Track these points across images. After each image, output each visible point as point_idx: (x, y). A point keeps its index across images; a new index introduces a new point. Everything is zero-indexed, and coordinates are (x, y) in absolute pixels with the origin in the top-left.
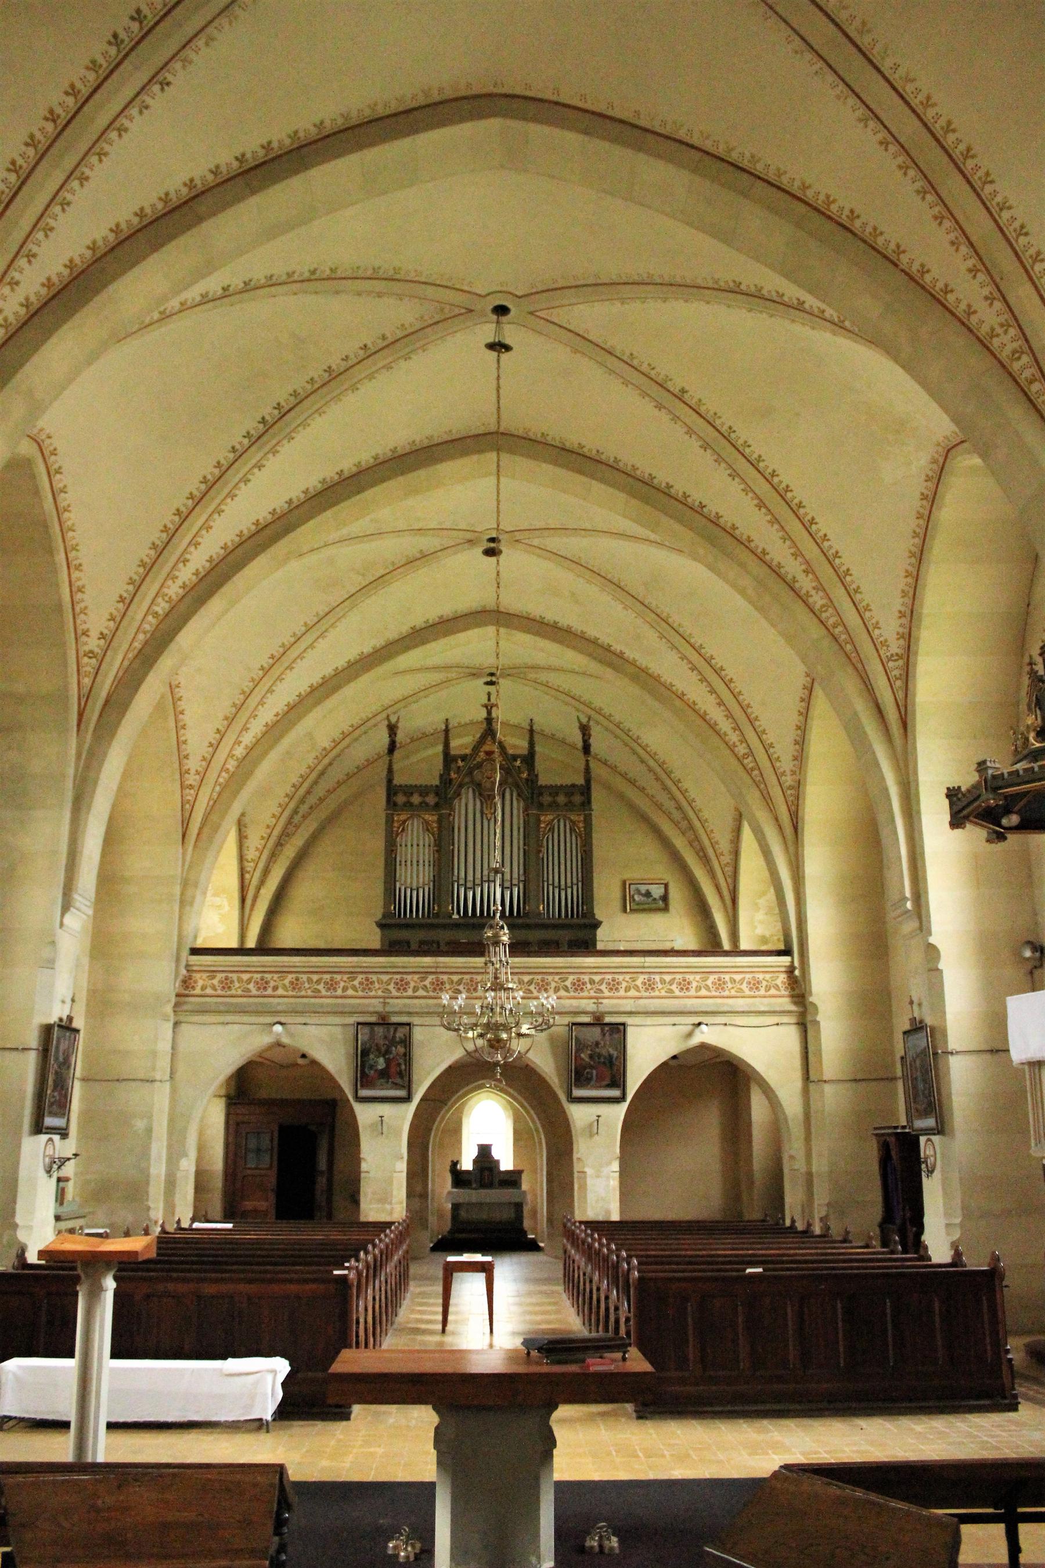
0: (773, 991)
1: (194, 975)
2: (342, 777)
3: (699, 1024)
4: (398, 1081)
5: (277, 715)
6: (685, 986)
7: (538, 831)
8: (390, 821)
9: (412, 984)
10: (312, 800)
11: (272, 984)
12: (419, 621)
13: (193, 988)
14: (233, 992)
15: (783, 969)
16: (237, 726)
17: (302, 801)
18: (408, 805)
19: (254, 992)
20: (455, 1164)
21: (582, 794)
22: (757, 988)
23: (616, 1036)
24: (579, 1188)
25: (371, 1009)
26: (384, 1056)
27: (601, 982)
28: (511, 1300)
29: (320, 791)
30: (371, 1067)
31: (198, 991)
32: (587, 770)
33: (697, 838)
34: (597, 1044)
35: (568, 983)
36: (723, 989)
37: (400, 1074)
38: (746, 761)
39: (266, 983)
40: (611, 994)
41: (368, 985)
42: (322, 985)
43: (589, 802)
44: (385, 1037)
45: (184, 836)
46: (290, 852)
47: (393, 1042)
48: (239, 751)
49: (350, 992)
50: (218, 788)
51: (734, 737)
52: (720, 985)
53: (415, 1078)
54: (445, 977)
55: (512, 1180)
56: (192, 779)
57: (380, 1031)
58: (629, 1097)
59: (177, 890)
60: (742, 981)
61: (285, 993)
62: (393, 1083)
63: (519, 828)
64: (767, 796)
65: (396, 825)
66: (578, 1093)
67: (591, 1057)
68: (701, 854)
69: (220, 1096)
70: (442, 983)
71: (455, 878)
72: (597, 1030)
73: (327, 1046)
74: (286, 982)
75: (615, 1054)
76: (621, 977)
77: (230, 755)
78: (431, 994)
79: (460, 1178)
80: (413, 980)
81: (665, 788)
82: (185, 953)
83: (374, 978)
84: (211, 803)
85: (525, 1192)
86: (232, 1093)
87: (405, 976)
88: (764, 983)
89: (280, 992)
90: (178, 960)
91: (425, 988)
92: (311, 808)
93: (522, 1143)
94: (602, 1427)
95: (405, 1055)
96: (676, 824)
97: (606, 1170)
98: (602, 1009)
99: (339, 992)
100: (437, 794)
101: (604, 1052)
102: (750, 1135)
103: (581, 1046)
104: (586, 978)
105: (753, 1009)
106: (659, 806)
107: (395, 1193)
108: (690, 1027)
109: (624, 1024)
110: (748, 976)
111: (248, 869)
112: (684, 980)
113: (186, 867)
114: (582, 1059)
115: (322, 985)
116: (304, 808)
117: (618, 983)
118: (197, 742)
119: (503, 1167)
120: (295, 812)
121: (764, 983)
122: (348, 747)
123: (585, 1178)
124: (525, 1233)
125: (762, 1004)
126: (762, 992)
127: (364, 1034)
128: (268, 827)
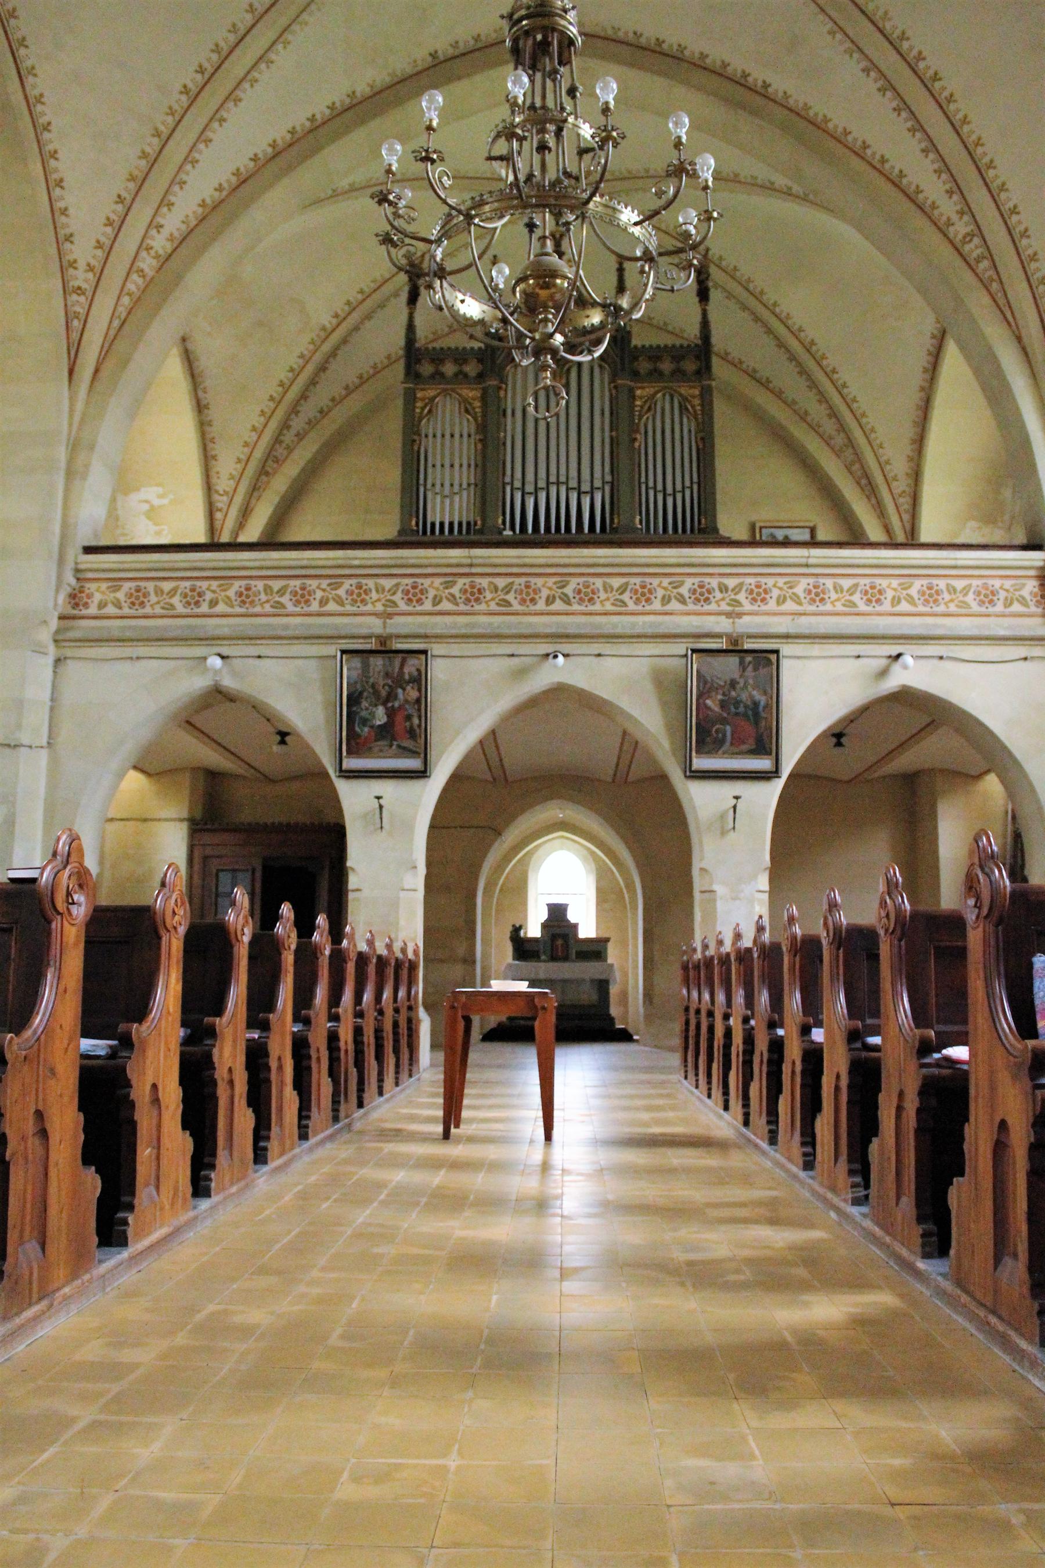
0: (1016, 607)
1: (87, 585)
2: (352, 379)
3: (899, 656)
4: (408, 743)
5: (220, 188)
6: (874, 596)
7: (632, 407)
8: (410, 398)
9: (432, 593)
10: (309, 410)
11: (209, 596)
12: (443, 46)
13: (86, 605)
14: (148, 610)
15: (1033, 573)
16: (154, 191)
17: (294, 410)
18: (438, 376)
19: (180, 609)
20: (516, 930)
21: (698, 357)
22: (991, 602)
23: (763, 671)
24: (703, 918)
25: (364, 631)
26: (384, 704)
27: (738, 589)
28: (590, 1091)
29: (321, 396)
30: (364, 722)
31: (93, 610)
32: (705, 324)
33: (858, 457)
34: (733, 684)
35: (684, 590)
36: (935, 601)
37: (412, 734)
38: (967, 248)
39: (200, 595)
40: (755, 608)
41: (360, 595)
42: (287, 596)
43: (708, 367)
44: (387, 675)
45: (71, 372)
46: (280, 484)
47: (400, 682)
48: (160, 243)
49: (332, 606)
50: (126, 300)
51: (948, 208)
52: (931, 596)
53: (435, 738)
54: (484, 582)
55: (595, 950)
56: (81, 278)
57: (377, 663)
58: (786, 770)
59: (62, 454)
60: (965, 591)
61: (229, 610)
62: (399, 746)
63: (603, 414)
64: (1002, 302)
65: (419, 404)
66: (700, 763)
67: (723, 705)
68: (864, 482)
69: (181, 820)
70: (480, 591)
71: (508, 479)
72: (733, 660)
73: (298, 694)
74: (231, 593)
75: (763, 700)
76: (770, 581)
77: (143, 246)
78: (462, 607)
79: (523, 949)
80: (433, 586)
81: (813, 385)
82: (74, 554)
83: (370, 583)
84: (116, 323)
85: (612, 966)
86: (198, 815)
87: (420, 581)
88: (1002, 595)
89: (221, 608)
90: (61, 561)
91: (453, 599)
92: (309, 422)
93: (606, 906)
94: (954, 1447)
95: (418, 701)
96: (827, 441)
97: (748, 890)
98: (740, 630)
99: (315, 606)
100: (480, 361)
101: (744, 696)
102: (937, 877)
103: (706, 688)
104: (714, 583)
105: (986, 633)
106: (803, 417)
107: (402, 922)
108: (884, 662)
109: (777, 652)
110: (975, 583)
111: (219, 505)
112: (873, 587)
113: (77, 418)
114: (708, 708)
115: (287, 596)
116: (298, 423)
117: (766, 591)
118: (87, 211)
119: (583, 934)
120: (285, 426)
121: (1002, 595)
122: (356, 329)
123: (715, 900)
124: (612, 1020)
125: (1001, 627)
126: (999, 608)
127: (350, 670)
128: (246, 444)
